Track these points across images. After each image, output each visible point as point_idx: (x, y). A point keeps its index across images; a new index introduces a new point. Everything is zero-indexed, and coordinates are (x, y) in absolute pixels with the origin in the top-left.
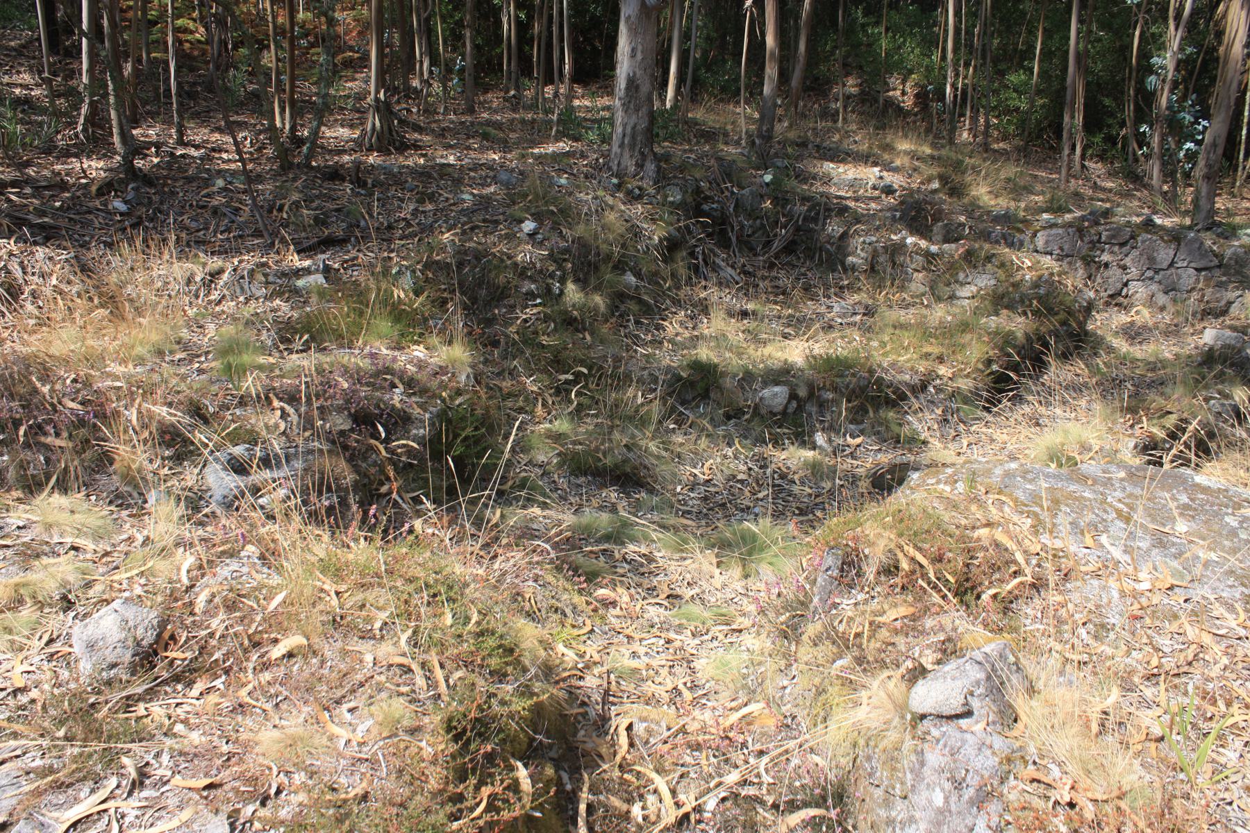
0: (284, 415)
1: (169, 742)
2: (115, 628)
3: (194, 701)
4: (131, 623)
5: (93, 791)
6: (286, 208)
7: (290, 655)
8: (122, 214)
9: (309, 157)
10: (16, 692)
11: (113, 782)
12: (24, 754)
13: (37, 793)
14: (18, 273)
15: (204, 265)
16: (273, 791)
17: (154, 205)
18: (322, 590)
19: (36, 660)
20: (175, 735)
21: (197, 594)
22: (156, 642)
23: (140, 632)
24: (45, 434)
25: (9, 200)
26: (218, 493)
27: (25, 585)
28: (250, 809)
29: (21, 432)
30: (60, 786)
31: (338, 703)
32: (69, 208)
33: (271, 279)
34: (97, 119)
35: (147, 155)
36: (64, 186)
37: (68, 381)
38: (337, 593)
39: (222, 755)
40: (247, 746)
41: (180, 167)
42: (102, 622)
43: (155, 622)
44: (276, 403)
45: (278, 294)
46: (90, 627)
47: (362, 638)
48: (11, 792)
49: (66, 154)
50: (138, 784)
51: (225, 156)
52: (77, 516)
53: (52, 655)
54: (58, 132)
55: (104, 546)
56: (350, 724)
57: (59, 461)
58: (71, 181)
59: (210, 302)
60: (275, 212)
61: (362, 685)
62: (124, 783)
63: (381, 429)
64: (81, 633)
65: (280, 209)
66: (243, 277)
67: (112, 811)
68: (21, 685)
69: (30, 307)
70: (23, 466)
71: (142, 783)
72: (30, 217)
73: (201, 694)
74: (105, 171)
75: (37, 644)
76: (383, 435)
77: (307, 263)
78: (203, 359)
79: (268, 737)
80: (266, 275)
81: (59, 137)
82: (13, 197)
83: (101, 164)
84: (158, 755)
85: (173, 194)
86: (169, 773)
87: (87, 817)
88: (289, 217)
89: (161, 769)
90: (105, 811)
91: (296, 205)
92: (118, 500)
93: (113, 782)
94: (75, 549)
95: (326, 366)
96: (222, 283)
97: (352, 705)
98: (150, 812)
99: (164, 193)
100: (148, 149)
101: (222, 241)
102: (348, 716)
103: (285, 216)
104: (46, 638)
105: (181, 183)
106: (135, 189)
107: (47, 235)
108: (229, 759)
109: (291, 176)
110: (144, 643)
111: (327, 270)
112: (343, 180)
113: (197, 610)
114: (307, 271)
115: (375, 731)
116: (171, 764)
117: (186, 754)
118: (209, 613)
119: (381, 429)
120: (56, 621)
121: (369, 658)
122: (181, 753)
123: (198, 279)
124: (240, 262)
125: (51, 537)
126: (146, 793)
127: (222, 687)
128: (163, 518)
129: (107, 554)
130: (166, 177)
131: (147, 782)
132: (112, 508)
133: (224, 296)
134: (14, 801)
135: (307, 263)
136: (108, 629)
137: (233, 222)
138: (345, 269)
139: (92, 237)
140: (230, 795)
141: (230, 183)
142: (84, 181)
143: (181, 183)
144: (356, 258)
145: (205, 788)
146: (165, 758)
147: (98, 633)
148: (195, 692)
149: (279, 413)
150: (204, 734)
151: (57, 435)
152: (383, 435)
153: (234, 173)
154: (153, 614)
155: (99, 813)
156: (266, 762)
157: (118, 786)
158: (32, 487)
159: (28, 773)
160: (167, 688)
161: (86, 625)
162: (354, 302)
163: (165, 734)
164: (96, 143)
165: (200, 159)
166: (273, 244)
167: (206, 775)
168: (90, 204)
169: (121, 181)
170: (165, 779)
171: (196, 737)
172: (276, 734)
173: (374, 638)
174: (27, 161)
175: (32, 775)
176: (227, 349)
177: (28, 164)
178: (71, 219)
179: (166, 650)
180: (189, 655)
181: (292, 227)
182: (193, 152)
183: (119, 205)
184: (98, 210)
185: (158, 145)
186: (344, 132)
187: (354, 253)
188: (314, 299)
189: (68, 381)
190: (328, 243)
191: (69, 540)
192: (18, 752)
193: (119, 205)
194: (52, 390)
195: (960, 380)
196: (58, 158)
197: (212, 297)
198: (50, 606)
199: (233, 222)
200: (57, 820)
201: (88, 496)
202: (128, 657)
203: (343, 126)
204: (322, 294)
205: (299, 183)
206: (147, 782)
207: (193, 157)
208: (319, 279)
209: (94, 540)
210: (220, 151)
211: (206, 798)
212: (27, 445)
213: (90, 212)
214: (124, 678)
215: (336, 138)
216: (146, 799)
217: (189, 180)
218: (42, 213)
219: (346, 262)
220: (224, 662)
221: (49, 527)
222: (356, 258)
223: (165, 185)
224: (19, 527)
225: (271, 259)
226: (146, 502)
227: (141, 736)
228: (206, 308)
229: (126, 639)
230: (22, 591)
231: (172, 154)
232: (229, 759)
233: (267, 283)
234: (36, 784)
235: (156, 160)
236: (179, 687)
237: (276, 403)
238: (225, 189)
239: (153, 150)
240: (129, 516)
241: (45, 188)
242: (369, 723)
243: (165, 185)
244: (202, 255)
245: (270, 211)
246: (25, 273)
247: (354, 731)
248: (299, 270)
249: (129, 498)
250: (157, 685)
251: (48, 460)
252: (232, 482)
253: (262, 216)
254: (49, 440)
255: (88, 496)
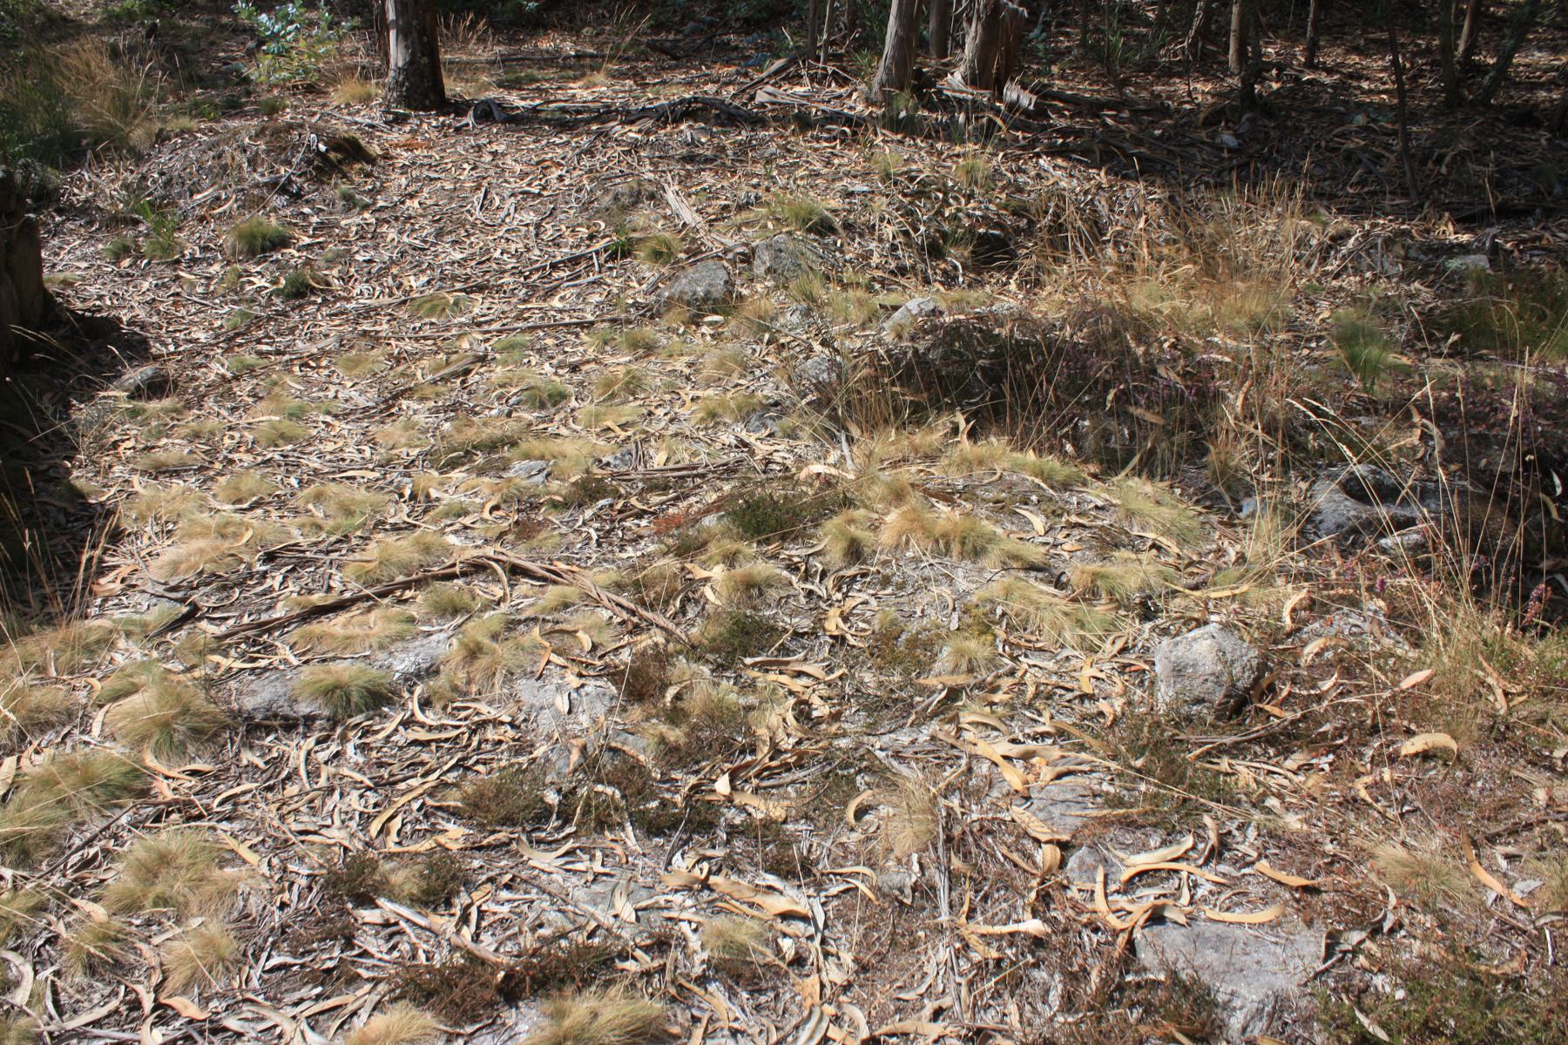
0: (1425, 437)
1: (1257, 816)
2: (1210, 657)
3: (1290, 775)
4: (1229, 656)
5: (1164, 843)
6: (1448, 159)
7: (1426, 756)
8: (1230, 150)
9: (1491, 91)
10: (1083, 697)
11: (1189, 841)
12: (1092, 771)
13: (1105, 822)
14: (1103, 208)
15: (1325, 224)
16: (1387, 926)
17: (1265, 142)
18: (1482, 683)
19: (1106, 667)
20: (1269, 811)
21: (1305, 644)
22: (1252, 687)
23: (1237, 670)
24: (1137, 404)
25: (1105, 125)
26: (1330, 520)
27: (1104, 576)
28: (1356, 937)
29: (1110, 397)
30: (1128, 824)
31: (1492, 839)
32: (1169, 138)
33: (1413, 253)
34: (1212, 34)
35: (1265, 79)
36: (1165, 112)
37: (1166, 345)
38: (1506, 694)
39: (1324, 855)
40: (1362, 855)
41: (1305, 97)
42: (1196, 646)
43: (1255, 663)
44: (1416, 419)
45: (1421, 275)
46: (1181, 647)
47: (1534, 764)
48: (1076, 811)
49: (1168, 73)
50: (1217, 854)
51: (1365, 85)
52: (1162, 509)
53: (1125, 666)
54: (1162, 47)
55: (1189, 553)
56: (1505, 875)
57: (1145, 438)
58: (1173, 105)
59: (1326, 274)
60: (1430, 165)
61: (1529, 826)
62: (1201, 846)
63: (1557, 481)
64: (1164, 652)
65: (1439, 161)
66: (1375, 246)
67: (1184, 875)
68: (1089, 691)
69: (1110, 251)
70: (1106, 436)
71: (1221, 854)
72: (1126, 145)
73: (1299, 768)
74: (1213, 96)
75: (1109, 648)
76: (1559, 491)
77: (1465, 238)
78: (1313, 345)
79: (1390, 852)
80: (1407, 248)
81: (1162, 52)
82: (1109, 121)
83: (1209, 87)
84: (1241, 827)
85: (1297, 129)
86: (1255, 854)
87: (1156, 870)
88: (1449, 173)
89: (1246, 845)
90: (1176, 871)
91: (1462, 157)
92: (1208, 500)
93: (1189, 841)
94: (1159, 548)
95: (1488, 382)
96: (1344, 250)
97: (1510, 849)
98: (1229, 893)
99: (1286, 128)
100: (1269, 71)
101: (1353, 196)
102: (1503, 863)
103: (1444, 170)
104: (1119, 644)
105: (1308, 116)
106: (1252, 121)
107: (1149, 170)
108: (1331, 863)
109: (1460, 116)
110: (1239, 684)
111: (1495, 249)
112: (1537, 125)
113: (1302, 662)
114: (1464, 249)
115: (1545, 896)
116: (1258, 843)
117: (1279, 838)
118: (1321, 667)
119: (1557, 481)
120: (1132, 628)
121: (1541, 795)
122: (1271, 835)
123: (1314, 242)
124: (1374, 226)
125: (1131, 526)
126: (1223, 868)
127: (1327, 767)
128: (1262, 537)
129: (1191, 563)
130: (1290, 108)
131: (1227, 855)
132: (1199, 508)
133: (1346, 267)
134: (1079, 822)
135: (1465, 238)
136: (1204, 652)
137: (1370, 172)
138: (1521, 252)
139: (1192, 175)
140: (1329, 909)
141: (1374, 121)
142: (1188, 107)
143: (1308, 116)
144: (1540, 238)
145: (1297, 889)
146: (1252, 833)
147: (1189, 657)
148: (1291, 763)
149: (1418, 432)
150: (1306, 821)
151: (1148, 408)
152: (1559, 491)
153: (1380, 107)
154: (1254, 653)
155: (1169, 871)
156: (1381, 885)
157: (1194, 848)
158: (1111, 463)
159: (1095, 796)
160: (1257, 749)
161: (1176, 644)
162: (1533, 299)
163: (1254, 805)
164: (1205, 62)
165: (1332, 87)
166: (1421, 206)
167: (1300, 873)
168: (1195, 135)
169: (1233, 109)
170: (1248, 859)
171: (1293, 822)
172: (1401, 852)
173: (1552, 768)
174: (1124, 80)
175: (1099, 800)
176: (1349, 337)
177: (1125, 82)
178: (1170, 152)
179: (1261, 701)
180: (1289, 716)
181: (1451, 186)
182: (1325, 78)
183: (1228, 138)
184: (1203, 143)
185: (1280, 68)
186: (1541, 57)
187: (1536, 231)
188: (1469, 288)
189: (1166, 345)
190: (1507, 213)
191: (1151, 535)
192: (1086, 768)
193: (1228, 138)
194: (1146, 353)
195: (151, 617)
196: (1158, 77)
197: (1329, 268)
198: (1127, 608)
199: (1370, 172)
200: (1122, 860)
201: (1171, 487)
202: (1218, 697)
203: (1540, 49)
204: (1481, 281)
205: (1470, 128)
206: (1227, 855)
207: (1323, 85)
208: (1481, 261)
209: (1178, 544)
210: (1360, 77)
211: (1298, 901)
212: (1111, 413)
213: (1192, 145)
214: (1210, 719)
215: (1527, 65)
216: (1224, 875)
217: (1319, 113)
218: (1138, 142)
219: (1524, 241)
220: (1334, 738)
221: (1130, 514)
222: (1540, 238)
223: (1288, 117)
224: (1097, 507)
225: (1413, 227)
226: (1240, 509)
227: (1227, 797)
228: (1319, 281)
229: (1222, 673)
230: (1099, 583)
231: (1297, 80)
232: (1331, 863)
233: (1406, 258)
234: (1105, 812)
235: (1275, 86)
236: (1271, 751)
237: (1416, 419)
238: (1366, 129)
239: (1274, 72)
240: (1221, 523)
241: (1146, 112)
242: (1533, 884)
243: (1288, 117)
244: (1322, 211)
245: (1424, 163)
246: (1111, 210)
247: (1510, 886)
248: (1453, 246)
249: (1224, 498)
250: (1249, 741)
251: (1132, 435)
252: (1349, 509)
253: (1411, 168)
254: (1137, 412)
255: (1171, 487)
